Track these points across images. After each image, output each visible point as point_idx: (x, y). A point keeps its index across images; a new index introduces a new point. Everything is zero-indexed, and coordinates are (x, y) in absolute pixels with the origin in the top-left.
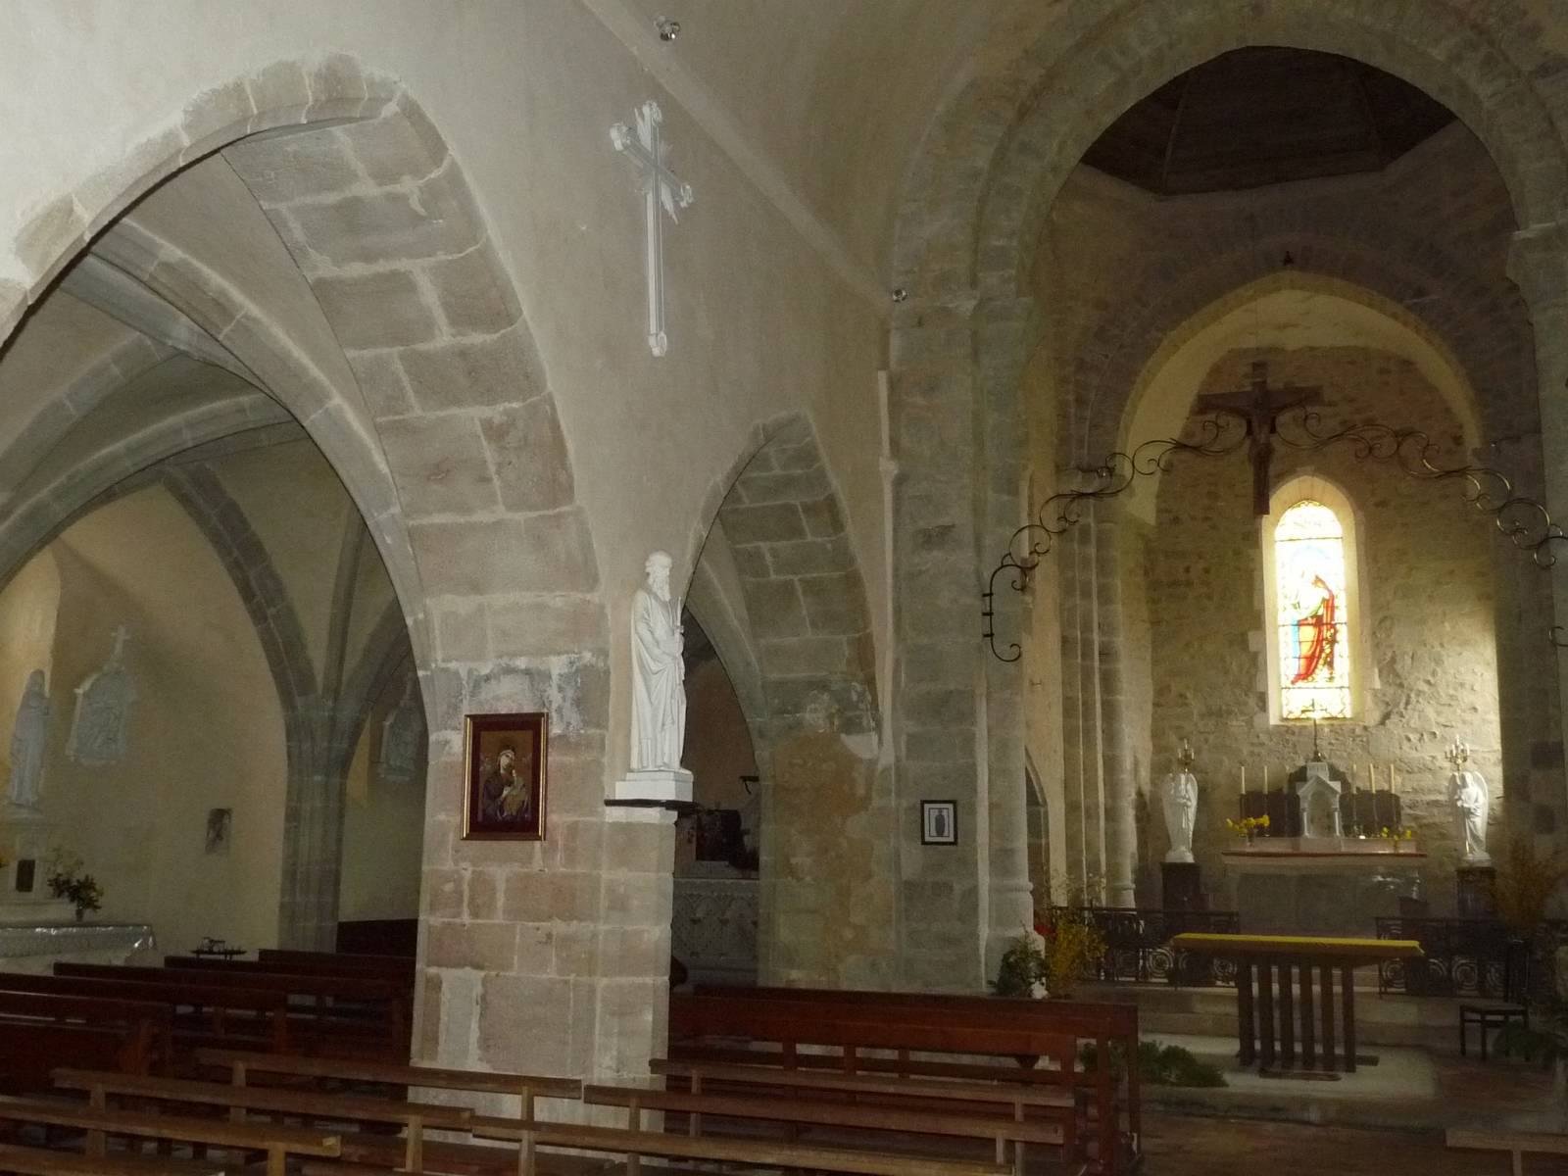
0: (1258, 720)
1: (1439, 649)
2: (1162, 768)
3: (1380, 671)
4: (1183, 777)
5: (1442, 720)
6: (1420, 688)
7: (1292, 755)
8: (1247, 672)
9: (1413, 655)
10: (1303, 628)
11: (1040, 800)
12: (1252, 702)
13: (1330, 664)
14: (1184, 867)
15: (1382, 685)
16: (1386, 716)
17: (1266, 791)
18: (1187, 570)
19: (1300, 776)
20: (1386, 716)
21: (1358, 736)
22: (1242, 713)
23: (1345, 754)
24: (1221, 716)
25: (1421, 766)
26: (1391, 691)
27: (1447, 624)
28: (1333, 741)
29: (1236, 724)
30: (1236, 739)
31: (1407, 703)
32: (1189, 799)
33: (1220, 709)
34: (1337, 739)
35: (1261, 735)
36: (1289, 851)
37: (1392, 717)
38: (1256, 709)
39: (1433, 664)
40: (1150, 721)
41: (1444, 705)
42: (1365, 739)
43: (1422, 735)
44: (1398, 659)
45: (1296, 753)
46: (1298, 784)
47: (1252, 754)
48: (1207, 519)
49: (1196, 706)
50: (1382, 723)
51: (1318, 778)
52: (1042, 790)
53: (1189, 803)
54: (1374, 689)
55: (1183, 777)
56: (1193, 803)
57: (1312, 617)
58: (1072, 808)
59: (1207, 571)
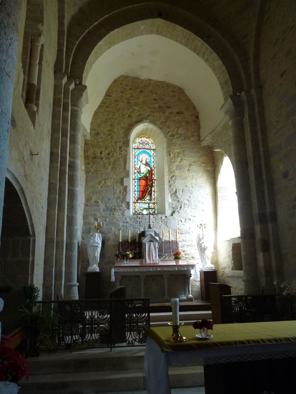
0: (126, 213)
1: (191, 188)
2: (87, 232)
3: (171, 195)
4: (97, 234)
5: (193, 214)
6: (185, 203)
7: (139, 227)
8: (123, 194)
9: (183, 190)
10: (141, 180)
11: (31, 233)
12: (124, 205)
13: (150, 195)
14: (94, 274)
15: (172, 201)
16: (173, 212)
17: (130, 241)
18: (101, 153)
19: (143, 234)
20: (173, 212)
21: (163, 220)
22: (120, 210)
23: (159, 227)
24: (112, 210)
25: (186, 231)
26: (175, 203)
27: (194, 180)
28: (154, 222)
29: (118, 214)
30: (117, 220)
31: (181, 208)
32: (99, 244)
33: (111, 208)
34: (156, 221)
35: (127, 219)
36: (139, 265)
37: (175, 212)
38: (126, 208)
39: (189, 194)
40: (83, 212)
41: (193, 209)
42: (166, 221)
43: (186, 220)
44: (177, 191)
45: (140, 226)
46: (142, 238)
47: (123, 226)
48: (110, 134)
49: (102, 206)
50: (172, 215)
51: (151, 235)
52: (32, 225)
53: (99, 246)
54: (169, 202)
55: (97, 234)
56: (100, 245)
57: (144, 177)
58: (49, 241)
59: (109, 154)
